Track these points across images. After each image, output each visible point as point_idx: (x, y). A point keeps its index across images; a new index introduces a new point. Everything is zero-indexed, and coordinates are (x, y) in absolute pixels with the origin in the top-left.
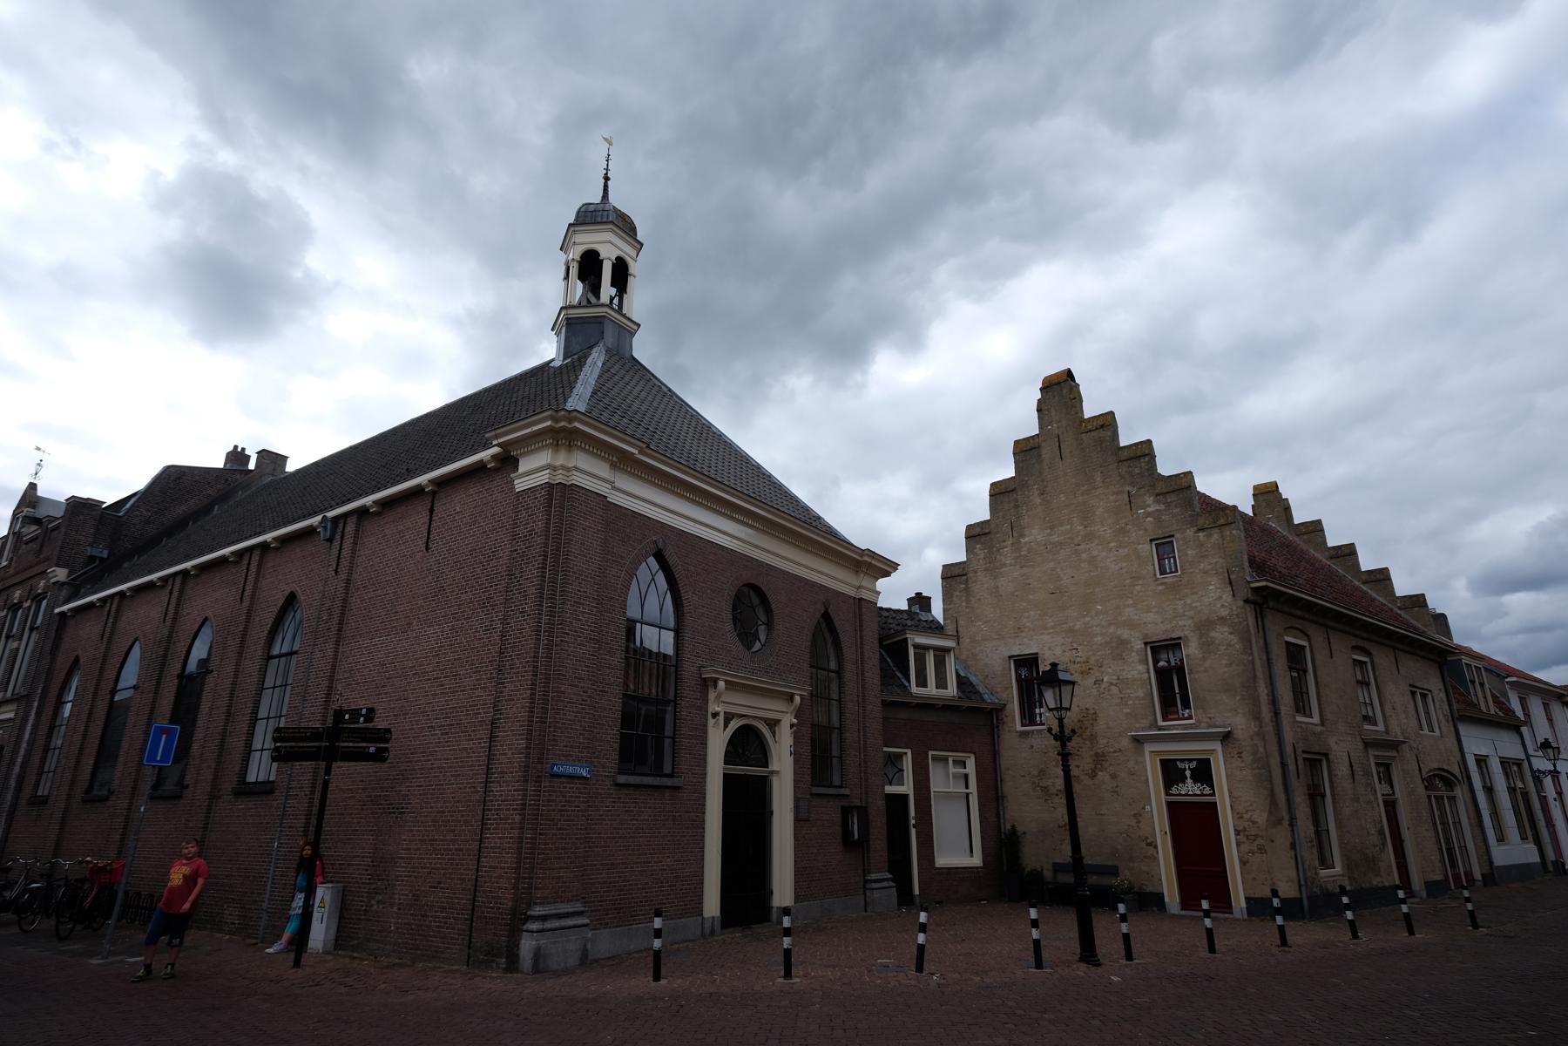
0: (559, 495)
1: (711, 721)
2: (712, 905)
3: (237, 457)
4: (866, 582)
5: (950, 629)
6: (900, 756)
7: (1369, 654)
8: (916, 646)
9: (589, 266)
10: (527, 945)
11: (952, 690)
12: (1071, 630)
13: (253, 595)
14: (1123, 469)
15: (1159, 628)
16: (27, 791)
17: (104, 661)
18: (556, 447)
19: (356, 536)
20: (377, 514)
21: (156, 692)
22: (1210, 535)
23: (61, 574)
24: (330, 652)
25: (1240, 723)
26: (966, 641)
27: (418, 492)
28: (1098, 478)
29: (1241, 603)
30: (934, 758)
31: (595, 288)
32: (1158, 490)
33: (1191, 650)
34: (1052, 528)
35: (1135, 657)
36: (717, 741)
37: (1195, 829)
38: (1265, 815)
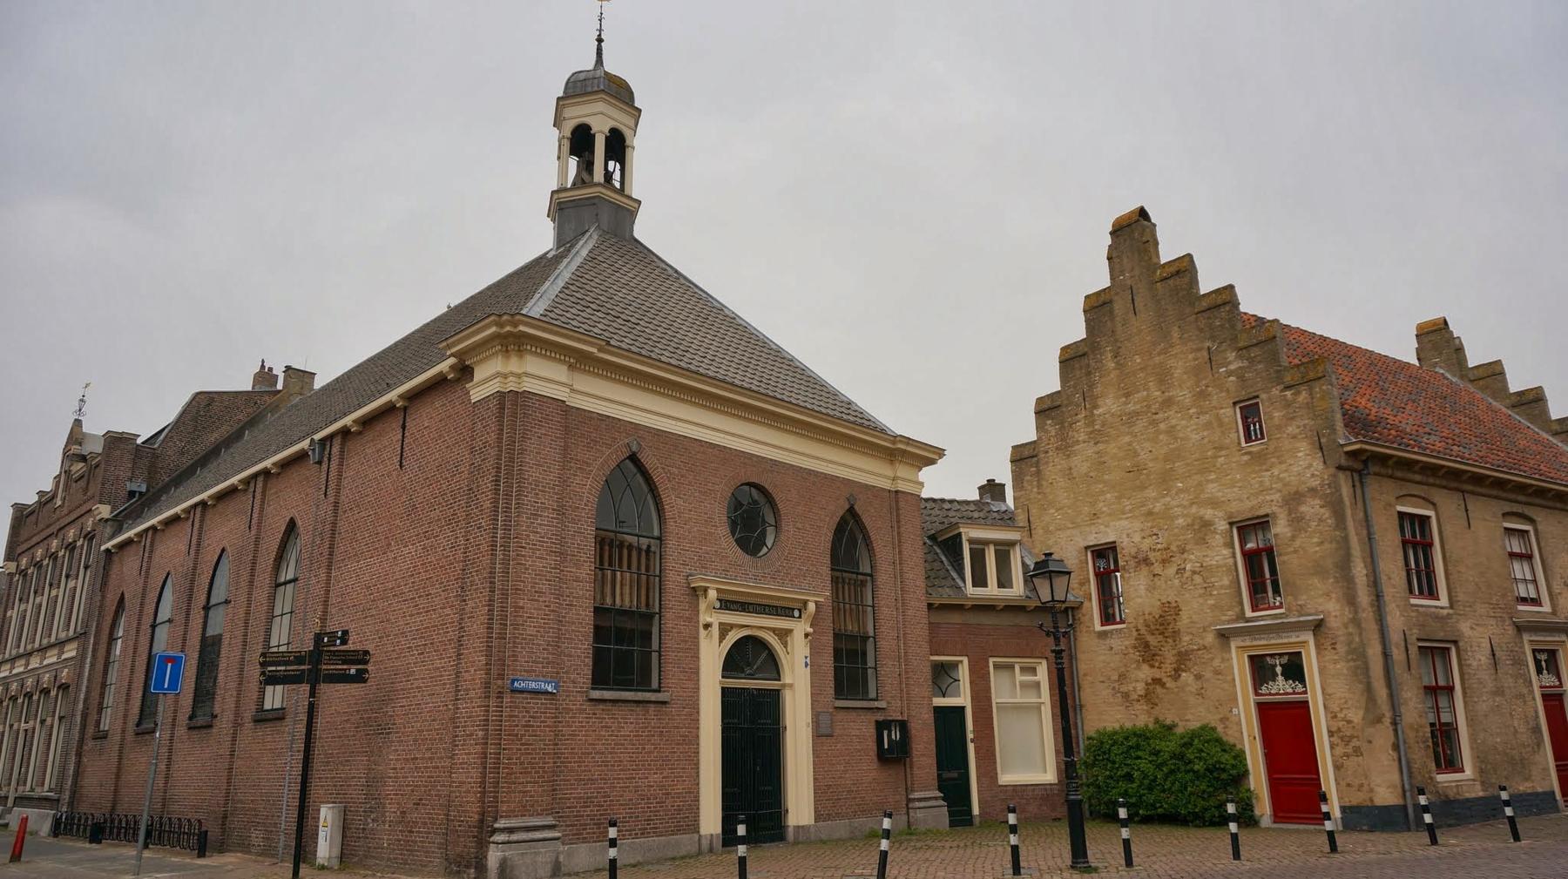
0: (512, 404)
1: (702, 632)
2: (711, 820)
3: (265, 375)
4: (903, 471)
5: (1021, 519)
6: (955, 665)
7: (1531, 521)
8: (971, 541)
9: (580, 142)
10: (494, 857)
11: (1018, 589)
12: (1150, 513)
13: (260, 523)
14: (1202, 323)
15: (1245, 506)
16: (90, 730)
17: (144, 596)
18: (506, 352)
19: (342, 458)
20: (360, 433)
21: (186, 625)
22: (1298, 393)
23: (105, 511)
24: (323, 577)
25: (1332, 608)
26: (1039, 532)
27: (390, 409)
28: (1175, 334)
29: (1332, 470)
30: (996, 666)
31: (587, 166)
32: (1241, 344)
33: (1281, 528)
34: (1127, 395)
35: (1219, 540)
36: (711, 656)
37: (1287, 727)
38: (1361, 713)
